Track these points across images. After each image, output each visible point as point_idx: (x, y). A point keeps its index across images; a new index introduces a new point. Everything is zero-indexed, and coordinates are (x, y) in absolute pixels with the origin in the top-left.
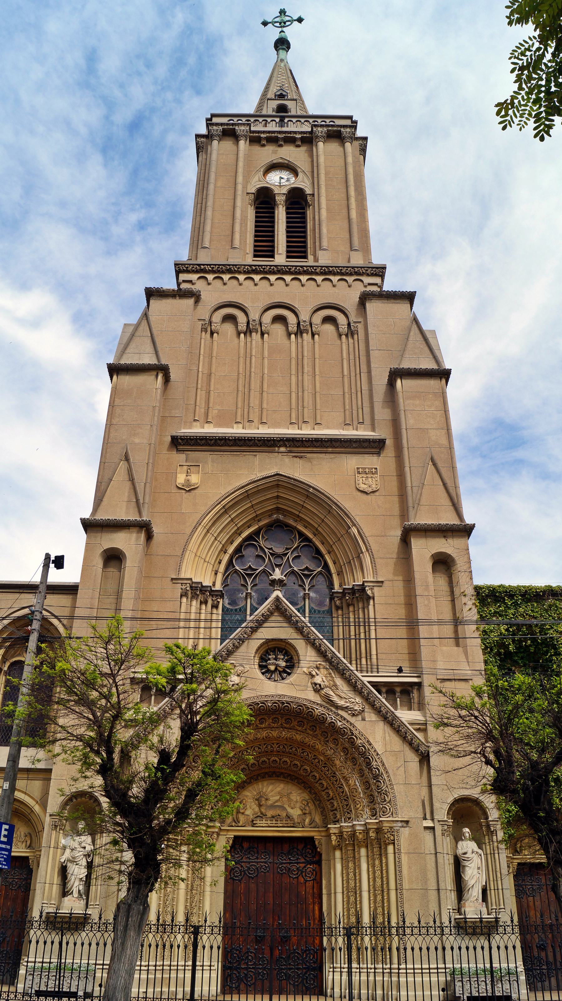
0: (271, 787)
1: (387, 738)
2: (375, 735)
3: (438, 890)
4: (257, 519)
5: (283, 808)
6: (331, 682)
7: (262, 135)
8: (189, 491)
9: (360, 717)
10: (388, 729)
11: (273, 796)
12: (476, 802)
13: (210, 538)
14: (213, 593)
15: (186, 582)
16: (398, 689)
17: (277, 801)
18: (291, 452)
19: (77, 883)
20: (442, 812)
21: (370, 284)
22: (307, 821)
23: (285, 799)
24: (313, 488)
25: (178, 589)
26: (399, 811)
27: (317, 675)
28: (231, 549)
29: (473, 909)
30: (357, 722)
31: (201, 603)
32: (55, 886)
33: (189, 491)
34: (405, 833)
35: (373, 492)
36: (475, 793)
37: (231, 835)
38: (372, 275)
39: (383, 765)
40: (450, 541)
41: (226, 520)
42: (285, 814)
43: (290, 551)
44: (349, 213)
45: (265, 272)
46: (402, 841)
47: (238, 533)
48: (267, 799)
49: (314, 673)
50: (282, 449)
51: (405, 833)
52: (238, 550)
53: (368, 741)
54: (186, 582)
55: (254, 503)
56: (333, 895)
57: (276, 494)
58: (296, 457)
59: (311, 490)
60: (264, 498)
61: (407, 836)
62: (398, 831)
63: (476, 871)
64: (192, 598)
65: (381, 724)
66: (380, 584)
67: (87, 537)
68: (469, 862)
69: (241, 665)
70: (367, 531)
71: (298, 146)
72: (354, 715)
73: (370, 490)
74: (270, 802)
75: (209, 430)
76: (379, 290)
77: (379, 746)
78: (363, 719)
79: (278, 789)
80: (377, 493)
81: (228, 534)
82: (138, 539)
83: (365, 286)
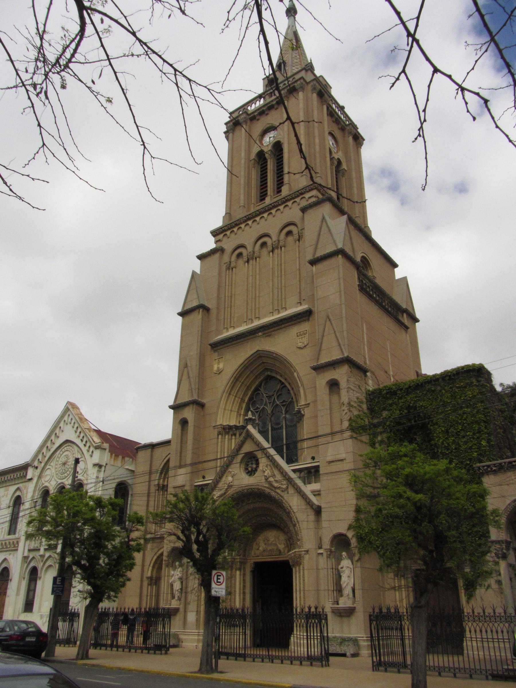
0: (270, 533)
2: (293, 502)
4: (256, 378)
5: (276, 545)
7: (264, 108)
8: (219, 373)
9: (286, 492)
10: (300, 497)
12: (345, 535)
13: (232, 398)
14: (236, 427)
16: (313, 470)
17: (273, 541)
18: (264, 334)
19: (176, 593)
20: (326, 544)
21: (310, 198)
22: (286, 551)
23: (277, 540)
25: (216, 431)
28: (246, 400)
29: (343, 601)
31: (232, 435)
32: (169, 595)
33: (219, 373)
34: (307, 557)
35: (305, 346)
36: (344, 531)
38: (310, 190)
39: (297, 519)
40: (337, 370)
41: (239, 384)
42: (275, 548)
43: (276, 392)
44: (231, 189)
45: (268, 209)
47: (248, 388)
48: (268, 541)
50: (260, 334)
51: (307, 557)
52: (251, 399)
55: (251, 370)
56: (242, 592)
57: (261, 362)
60: (256, 366)
62: (303, 557)
63: (346, 579)
64: (225, 434)
65: (296, 494)
70: (301, 374)
71: (276, 109)
72: (283, 491)
73: (303, 345)
74: (270, 542)
75: (232, 332)
76: (317, 199)
77: (295, 508)
78: (288, 493)
80: (307, 347)
82: (193, 409)
83: (307, 201)
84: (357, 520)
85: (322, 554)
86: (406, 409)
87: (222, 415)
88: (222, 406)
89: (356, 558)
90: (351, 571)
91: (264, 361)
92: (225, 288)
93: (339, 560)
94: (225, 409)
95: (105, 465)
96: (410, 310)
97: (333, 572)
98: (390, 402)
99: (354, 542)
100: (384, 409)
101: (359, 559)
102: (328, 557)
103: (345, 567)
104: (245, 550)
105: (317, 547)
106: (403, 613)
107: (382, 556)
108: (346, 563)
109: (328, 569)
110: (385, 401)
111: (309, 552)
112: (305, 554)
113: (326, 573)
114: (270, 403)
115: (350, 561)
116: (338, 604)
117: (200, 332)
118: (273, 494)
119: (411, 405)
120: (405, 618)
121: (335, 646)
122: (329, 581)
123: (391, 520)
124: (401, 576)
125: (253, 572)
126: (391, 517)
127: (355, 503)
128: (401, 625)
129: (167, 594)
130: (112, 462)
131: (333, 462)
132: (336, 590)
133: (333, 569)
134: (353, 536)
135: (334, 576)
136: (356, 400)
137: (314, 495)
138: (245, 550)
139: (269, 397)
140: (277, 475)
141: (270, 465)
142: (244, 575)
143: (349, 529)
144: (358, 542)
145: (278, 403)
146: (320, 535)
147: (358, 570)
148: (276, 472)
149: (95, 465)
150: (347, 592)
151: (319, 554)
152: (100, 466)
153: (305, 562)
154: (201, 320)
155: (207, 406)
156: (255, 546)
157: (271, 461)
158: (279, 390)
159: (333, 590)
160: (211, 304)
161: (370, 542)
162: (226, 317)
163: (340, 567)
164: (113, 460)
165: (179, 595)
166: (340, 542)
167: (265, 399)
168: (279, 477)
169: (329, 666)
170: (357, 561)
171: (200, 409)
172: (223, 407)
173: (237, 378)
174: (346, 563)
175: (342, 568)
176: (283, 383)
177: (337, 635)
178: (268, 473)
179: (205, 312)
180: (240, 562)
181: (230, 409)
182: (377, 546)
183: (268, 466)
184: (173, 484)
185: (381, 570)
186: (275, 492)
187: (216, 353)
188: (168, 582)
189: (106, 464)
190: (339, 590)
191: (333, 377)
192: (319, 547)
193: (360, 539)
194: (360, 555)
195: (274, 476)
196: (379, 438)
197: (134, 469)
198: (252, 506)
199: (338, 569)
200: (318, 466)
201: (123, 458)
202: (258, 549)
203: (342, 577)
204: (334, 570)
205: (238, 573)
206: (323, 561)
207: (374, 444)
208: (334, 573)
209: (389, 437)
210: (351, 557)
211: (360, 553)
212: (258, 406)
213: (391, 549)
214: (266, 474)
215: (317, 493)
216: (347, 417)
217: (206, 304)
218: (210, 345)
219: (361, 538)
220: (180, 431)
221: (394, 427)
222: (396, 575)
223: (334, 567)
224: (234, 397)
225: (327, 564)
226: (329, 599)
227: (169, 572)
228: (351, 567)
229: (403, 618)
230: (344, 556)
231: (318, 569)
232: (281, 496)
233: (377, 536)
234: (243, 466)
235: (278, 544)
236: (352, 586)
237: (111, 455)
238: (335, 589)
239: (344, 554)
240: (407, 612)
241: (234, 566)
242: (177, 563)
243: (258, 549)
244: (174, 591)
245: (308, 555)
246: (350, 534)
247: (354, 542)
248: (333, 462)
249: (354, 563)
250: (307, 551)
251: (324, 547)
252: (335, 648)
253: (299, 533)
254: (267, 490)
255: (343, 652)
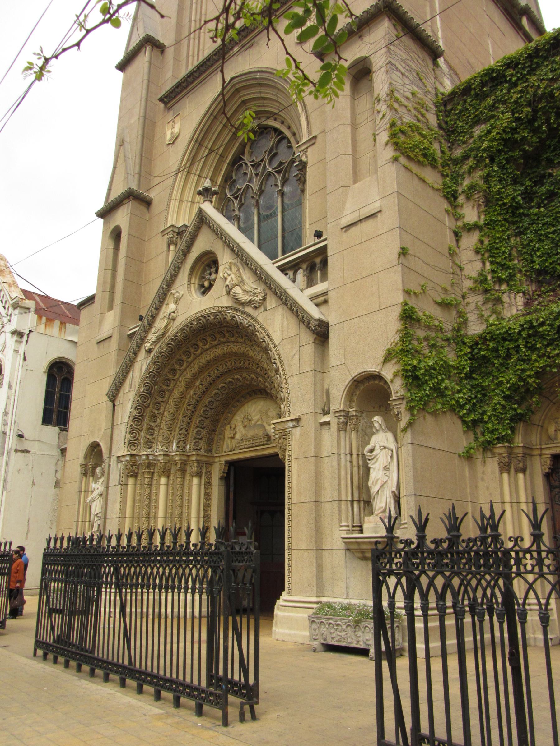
1: (285, 323)
2: (275, 326)
3: (317, 502)
6: (240, 279)
9: (262, 309)
10: (287, 312)
11: (255, 416)
12: (378, 377)
15: (169, 230)
17: (258, 421)
20: (338, 402)
24: (259, 72)
26: (292, 410)
27: (229, 275)
29: (372, 525)
30: (260, 316)
34: (297, 432)
36: (373, 366)
37: (547, 453)
39: (279, 358)
42: (261, 433)
46: (293, 446)
49: (226, 275)
51: (297, 432)
53: (268, 334)
54: (169, 230)
56: (202, 515)
57: (240, 101)
58: (247, 49)
59: (258, 75)
61: (298, 436)
65: (280, 309)
66: (313, 141)
67: (105, 223)
68: (373, 461)
69: (177, 292)
72: (256, 308)
77: (277, 337)
78: (265, 310)
79: (259, 407)
81: (211, 166)
84: (406, 336)
85: (328, 423)
86: (529, 104)
87: (176, 210)
88: (176, 194)
89: (403, 424)
90: (392, 457)
91: (244, 98)
92: (191, 8)
93: (366, 434)
94: (181, 201)
95: (27, 332)
96: (533, 9)
97: (351, 462)
98: (490, 101)
99: (397, 388)
100: (477, 122)
101: (410, 424)
102: (343, 427)
103: (377, 447)
104: (210, 442)
105: (320, 411)
106: (517, 540)
107: (472, 426)
108: (382, 439)
109: (339, 454)
110: (479, 105)
111: (302, 423)
112: (294, 427)
113: (335, 464)
114: (257, 175)
115: (390, 435)
116: (361, 531)
117: (146, 82)
118: (240, 318)
119: (540, 92)
120: (529, 562)
121: (344, 630)
122: (343, 482)
123: (492, 345)
124: (517, 471)
125: (225, 479)
126: (492, 339)
127: (401, 300)
128: (509, 595)
129: (84, 522)
130: (42, 328)
131: (354, 224)
132: (359, 501)
133: (351, 454)
134: (395, 375)
135: (355, 469)
136: (409, 95)
137: (317, 305)
138: (210, 442)
139: (256, 166)
140: (247, 280)
141: (235, 265)
142: (208, 484)
143: (386, 360)
144: (407, 387)
145: (270, 170)
146: (326, 387)
147: (406, 451)
148: (246, 275)
149: (14, 333)
150: (383, 505)
151: (322, 424)
152: (20, 335)
153: (293, 443)
154: (147, 64)
155: (155, 202)
156: (228, 433)
157: (237, 255)
158: (271, 150)
159: (352, 502)
160: (166, 39)
161: (439, 391)
162: (191, 53)
163: (367, 448)
164: (43, 326)
165: (99, 522)
166: (369, 392)
167: (250, 170)
168: (251, 283)
169: (254, 717)
170: (404, 430)
171: (143, 209)
172: (178, 197)
173: (199, 140)
174: (382, 439)
175: (372, 451)
176: (281, 133)
177: (354, 602)
178: (232, 278)
179: (156, 51)
180: (197, 461)
181: (190, 199)
182: (457, 402)
183: (233, 267)
184: (97, 338)
185: (468, 457)
186: (243, 313)
187: (171, 113)
188: (85, 501)
189: (30, 331)
190: (366, 503)
191: (358, 56)
192: (323, 410)
193: (413, 378)
194: (412, 415)
195: (241, 282)
196: (466, 182)
197: (76, 340)
198: (211, 355)
199: (363, 455)
200: (325, 247)
201: (63, 324)
202: (233, 438)
203: (371, 471)
204: (354, 456)
205: (195, 481)
206: (329, 438)
207: (456, 198)
208: (355, 463)
209: (488, 175)
210: (391, 428)
211: (411, 409)
212: (238, 186)
213: (494, 410)
214: (227, 283)
215: (322, 299)
216: (385, 124)
217: (160, 39)
218: (161, 100)
219: (416, 378)
220: (111, 251)
221: (499, 151)
222: (505, 467)
223: (354, 451)
224: (196, 177)
225: (339, 444)
226: (340, 521)
227: (87, 485)
228: (393, 446)
229: (518, 562)
230: (376, 425)
231: (318, 457)
232: (252, 318)
233: (460, 383)
234: (195, 281)
235: (265, 424)
236: (394, 489)
237: (40, 317)
238: (356, 498)
239: (377, 419)
240: (537, 538)
241: (188, 469)
242: (98, 470)
243: (233, 438)
244: (92, 516)
245: (298, 429)
246: (388, 372)
247: (397, 388)
248: (354, 224)
249: (399, 434)
250: (298, 420)
251: (333, 408)
252: (343, 634)
253: (284, 385)
254: (230, 313)
255: (362, 646)
